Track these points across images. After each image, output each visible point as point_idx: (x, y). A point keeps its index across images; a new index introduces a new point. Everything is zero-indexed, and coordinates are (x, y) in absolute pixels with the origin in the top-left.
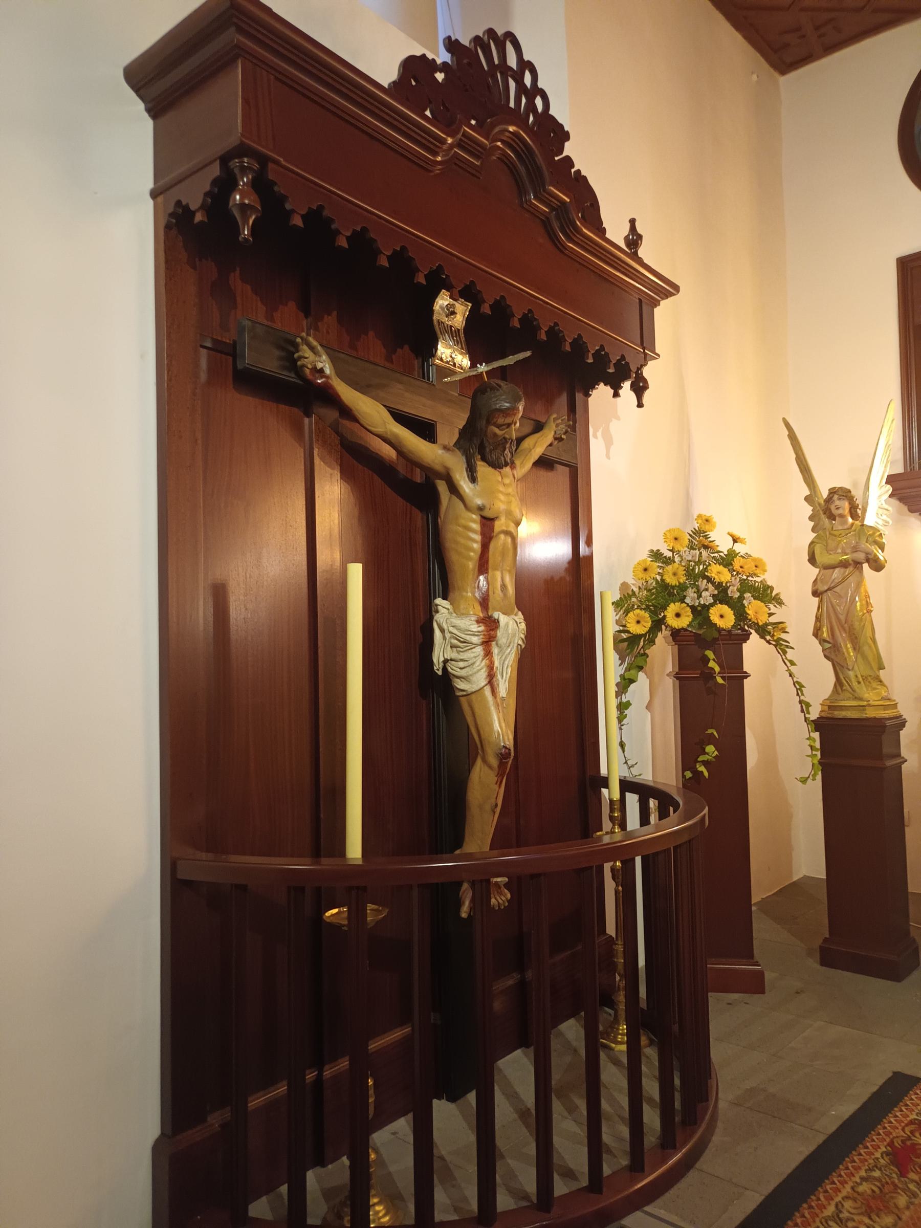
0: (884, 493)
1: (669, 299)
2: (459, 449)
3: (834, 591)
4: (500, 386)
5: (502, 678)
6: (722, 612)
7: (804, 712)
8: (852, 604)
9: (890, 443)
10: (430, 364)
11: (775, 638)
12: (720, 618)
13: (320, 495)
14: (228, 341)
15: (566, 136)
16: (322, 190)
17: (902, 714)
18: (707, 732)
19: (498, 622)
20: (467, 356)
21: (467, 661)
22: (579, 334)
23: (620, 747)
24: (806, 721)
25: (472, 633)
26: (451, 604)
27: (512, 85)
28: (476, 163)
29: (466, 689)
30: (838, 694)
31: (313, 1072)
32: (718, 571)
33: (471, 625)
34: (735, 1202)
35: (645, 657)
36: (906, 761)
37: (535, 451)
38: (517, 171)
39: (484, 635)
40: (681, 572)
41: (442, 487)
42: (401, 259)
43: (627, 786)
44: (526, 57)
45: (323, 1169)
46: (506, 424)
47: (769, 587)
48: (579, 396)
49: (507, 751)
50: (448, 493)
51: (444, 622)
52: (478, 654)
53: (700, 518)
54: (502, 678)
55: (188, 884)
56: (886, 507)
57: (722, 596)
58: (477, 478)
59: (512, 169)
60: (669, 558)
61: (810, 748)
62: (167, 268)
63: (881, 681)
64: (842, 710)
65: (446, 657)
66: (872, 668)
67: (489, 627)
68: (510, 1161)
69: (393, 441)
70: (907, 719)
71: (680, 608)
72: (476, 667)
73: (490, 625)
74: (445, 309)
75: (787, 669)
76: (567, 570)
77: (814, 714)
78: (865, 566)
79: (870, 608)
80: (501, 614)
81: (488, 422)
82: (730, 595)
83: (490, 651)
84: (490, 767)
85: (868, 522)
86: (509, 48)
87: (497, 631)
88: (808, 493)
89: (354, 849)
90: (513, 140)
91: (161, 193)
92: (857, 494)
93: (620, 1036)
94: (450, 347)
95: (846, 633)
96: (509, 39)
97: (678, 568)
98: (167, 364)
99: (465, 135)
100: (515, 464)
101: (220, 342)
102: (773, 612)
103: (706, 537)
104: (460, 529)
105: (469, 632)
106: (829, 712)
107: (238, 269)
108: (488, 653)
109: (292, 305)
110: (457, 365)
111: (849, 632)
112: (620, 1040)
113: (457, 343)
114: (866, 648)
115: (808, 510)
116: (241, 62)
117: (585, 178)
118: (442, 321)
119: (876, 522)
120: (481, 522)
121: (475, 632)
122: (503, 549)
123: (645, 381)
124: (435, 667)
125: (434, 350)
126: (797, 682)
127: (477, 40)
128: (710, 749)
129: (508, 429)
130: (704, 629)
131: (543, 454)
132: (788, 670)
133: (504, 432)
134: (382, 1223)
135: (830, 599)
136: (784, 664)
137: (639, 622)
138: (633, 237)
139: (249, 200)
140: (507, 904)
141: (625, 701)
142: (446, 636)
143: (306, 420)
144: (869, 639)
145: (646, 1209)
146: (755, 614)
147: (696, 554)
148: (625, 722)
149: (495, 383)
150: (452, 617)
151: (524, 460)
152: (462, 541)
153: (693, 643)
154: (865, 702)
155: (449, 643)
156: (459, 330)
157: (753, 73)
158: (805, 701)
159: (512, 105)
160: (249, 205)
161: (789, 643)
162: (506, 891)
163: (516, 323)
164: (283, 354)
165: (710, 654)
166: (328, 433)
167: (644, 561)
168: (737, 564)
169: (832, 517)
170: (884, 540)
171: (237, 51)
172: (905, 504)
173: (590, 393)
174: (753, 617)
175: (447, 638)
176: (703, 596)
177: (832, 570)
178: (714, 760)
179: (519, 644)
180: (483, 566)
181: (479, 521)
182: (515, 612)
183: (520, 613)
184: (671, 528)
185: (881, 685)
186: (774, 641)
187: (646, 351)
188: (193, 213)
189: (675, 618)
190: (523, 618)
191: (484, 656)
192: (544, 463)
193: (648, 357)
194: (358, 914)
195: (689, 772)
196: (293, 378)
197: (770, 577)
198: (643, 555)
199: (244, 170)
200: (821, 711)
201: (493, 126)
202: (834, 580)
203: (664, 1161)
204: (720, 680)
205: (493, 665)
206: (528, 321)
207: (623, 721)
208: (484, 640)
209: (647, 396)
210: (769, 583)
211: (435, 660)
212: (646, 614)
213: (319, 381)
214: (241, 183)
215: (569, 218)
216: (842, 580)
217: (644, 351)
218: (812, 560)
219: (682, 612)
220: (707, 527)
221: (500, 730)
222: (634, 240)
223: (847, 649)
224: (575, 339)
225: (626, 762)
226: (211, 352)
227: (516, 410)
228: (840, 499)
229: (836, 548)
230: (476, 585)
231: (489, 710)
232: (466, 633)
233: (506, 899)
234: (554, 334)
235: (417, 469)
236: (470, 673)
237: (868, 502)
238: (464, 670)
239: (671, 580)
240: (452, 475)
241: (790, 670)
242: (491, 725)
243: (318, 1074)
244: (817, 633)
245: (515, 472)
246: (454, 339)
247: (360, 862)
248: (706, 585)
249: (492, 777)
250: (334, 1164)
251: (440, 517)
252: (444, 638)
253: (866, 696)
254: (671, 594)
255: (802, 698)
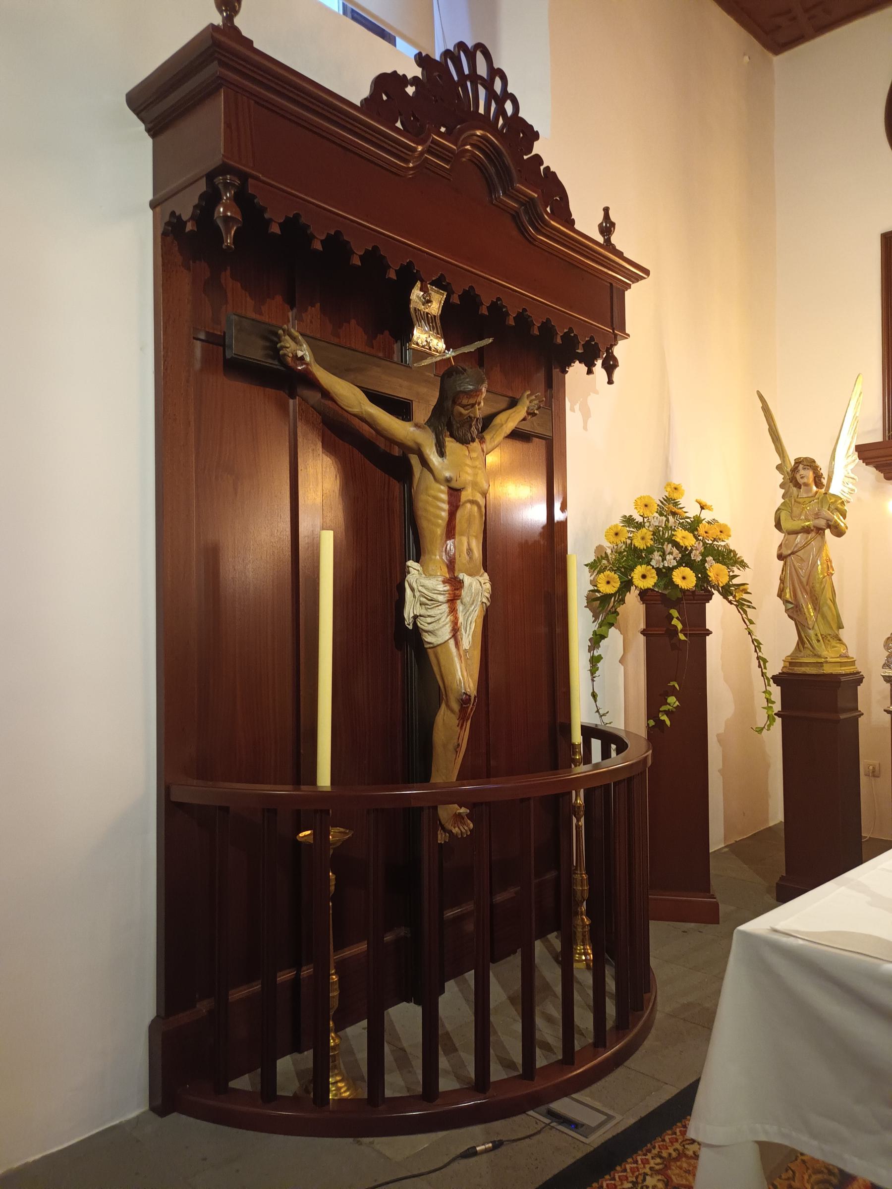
0: (851, 463)
1: (640, 282)
2: (429, 426)
3: (797, 555)
4: (465, 370)
5: (466, 633)
6: (684, 574)
7: (761, 668)
8: (813, 567)
9: (857, 415)
10: (408, 348)
11: (737, 599)
12: (682, 579)
13: (303, 468)
14: (219, 333)
15: (536, 136)
16: (298, 200)
17: (859, 671)
18: (669, 684)
19: (463, 582)
20: (443, 340)
21: (434, 617)
22: (547, 318)
23: (592, 697)
24: (763, 676)
25: (438, 592)
26: (421, 566)
27: (482, 92)
28: (447, 166)
29: (432, 642)
30: (800, 651)
31: (292, 972)
32: (684, 536)
33: (438, 585)
34: (653, 1093)
35: (615, 615)
36: (862, 714)
37: (506, 426)
38: (486, 169)
39: (449, 594)
40: (649, 536)
41: (414, 460)
42: (374, 258)
43: (589, 732)
44: (496, 66)
45: (299, 1055)
46: (470, 404)
47: (731, 551)
48: (556, 372)
49: (468, 697)
50: (420, 465)
51: (415, 582)
52: (443, 611)
53: (669, 486)
54: (466, 633)
55: (180, 805)
56: (852, 476)
57: (686, 560)
58: (445, 452)
59: (481, 167)
60: (641, 523)
61: (766, 700)
62: (163, 271)
63: (840, 640)
64: (801, 666)
65: (415, 613)
66: (831, 628)
67: (454, 586)
68: (462, 1054)
69: (368, 420)
70: (864, 676)
71: (646, 570)
72: (441, 622)
73: (455, 585)
74: (422, 298)
75: (746, 627)
76: (541, 534)
77: (775, 668)
78: (827, 531)
79: (831, 571)
80: (465, 575)
81: (454, 402)
82: (693, 558)
83: (455, 608)
84: (452, 711)
85: (832, 491)
86: (480, 57)
87: (461, 591)
88: (779, 462)
89: (324, 778)
90: (481, 142)
91: (159, 205)
92: (823, 465)
93: (577, 956)
94: (426, 332)
95: (807, 594)
96: (479, 50)
97: (646, 533)
98: (164, 356)
99: (434, 142)
100: (484, 438)
101: (213, 334)
102: (737, 574)
103: (676, 504)
104: (430, 499)
105: (436, 592)
106: (790, 668)
107: (229, 268)
108: (453, 610)
109: (279, 299)
110: (433, 348)
111: (810, 594)
112: (577, 958)
113: (432, 328)
114: (825, 609)
115: (779, 478)
116: (224, 91)
117: (554, 173)
118: (418, 309)
119: (842, 490)
120: (448, 493)
121: (441, 591)
122: (470, 515)
123: (615, 359)
124: (406, 622)
125: (411, 335)
126: (755, 639)
127: (447, 53)
128: (672, 700)
129: (473, 409)
130: (669, 589)
131: (516, 428)
132: (748, 628)
133: (469, 411)
134: (342, 1097)
135: (793, 563)
136: (743, 623)
137: (609, 584)
138: (606, 225)
139: (231, 213)
140: (469, 833)
141: (596, 655)
142: (416, 594)
143: (291, 401)
144: (829, 600)
145: (574, 1096)
146: (716, 576)
147: (662, 520)
148: (597, 674)
149: (462, 368)
150: (421, 578)
151: (494, 435)
152: (432, 509)
153: (660, 602)
154: (823, 659)
155: (419, 601)
156: (435, 316)
157: (745, 55)
158: (763, 657)
159: (481, 110)
160: (230, 217)
161: (751, 603)
162: (469, 821)
163: (484, 311)
164: (268, 344)
165: (674, 613)
166: (311, 413)
167: (616, 526)
168: (701, 529)
169: (798, 486)
170: (846, 508)
171: (219, 81)
172: (881, 471)
173: (567, 369)
174: (713, 579)
175: (417, 597)
176: (667, 559)
177: (796, 535)
178: (674, 710)
179: (483, 603)
180: (450, 532)
181: (447, 492)
182: (482, 573)
183: (486, 574)
184: (642, 495)
185: (840, 643)
186: (736, 601)
187: (616, 332)
188: (185, 223)
189: (642, 579)
190: (488, 579)
191: (449, 612)
192: (516, 435)
193: (618, 337)
194: (321, 835)
195: (652, 720)
196: (277, 365)
197: (733, 543)
198: (617, 521)
199: (227, 186)
200: (783, 667)
201: (462, 131)
202: (797, 544)
203: (595, 1057)
204: (682, 637)
205: (458, 620)
206: (496, 308)
207: (595, 673)
208: (449, 598)
209: (617, 373)
210: (732, 548)
211: (406, 616)
212: (616, 575)
213: (299, 368)
214: (225, 198)
215: (537, 214)
216: (805, 544)
217: (614, 331)
218: (778, 526)
219: (648, 574)
220: (675, 495)
221: (461, 678)
222: (607, 227)
223: (808, 609)
224: (543, 323)
225: (598, 711)
226: (204, 343)
227: (479, 392)
228: (805, 469)
229: (800, 515)
230: (444, 549)
231: (453, 661)
232: (433, 592)
233: (469, 828)
234: (523, 319)
235: (395, 446)
236: (436, 628)
237: (833, 471)
238: (431, 625)
239: (639, 544)
240: (423, 449)
241: (749, 629)
242: (454, 674)
243: (296, 973)
244: (780, 594)
245: (484, 446)
246: (430, 326)
247: (329, 789)
248: (671, 549)
249: (454, 720)
250: (308, 1051)
251: (413, 488)
252: (414, 596)
253: (825, 653)
254: (640, 557)
255: (760, 654)
